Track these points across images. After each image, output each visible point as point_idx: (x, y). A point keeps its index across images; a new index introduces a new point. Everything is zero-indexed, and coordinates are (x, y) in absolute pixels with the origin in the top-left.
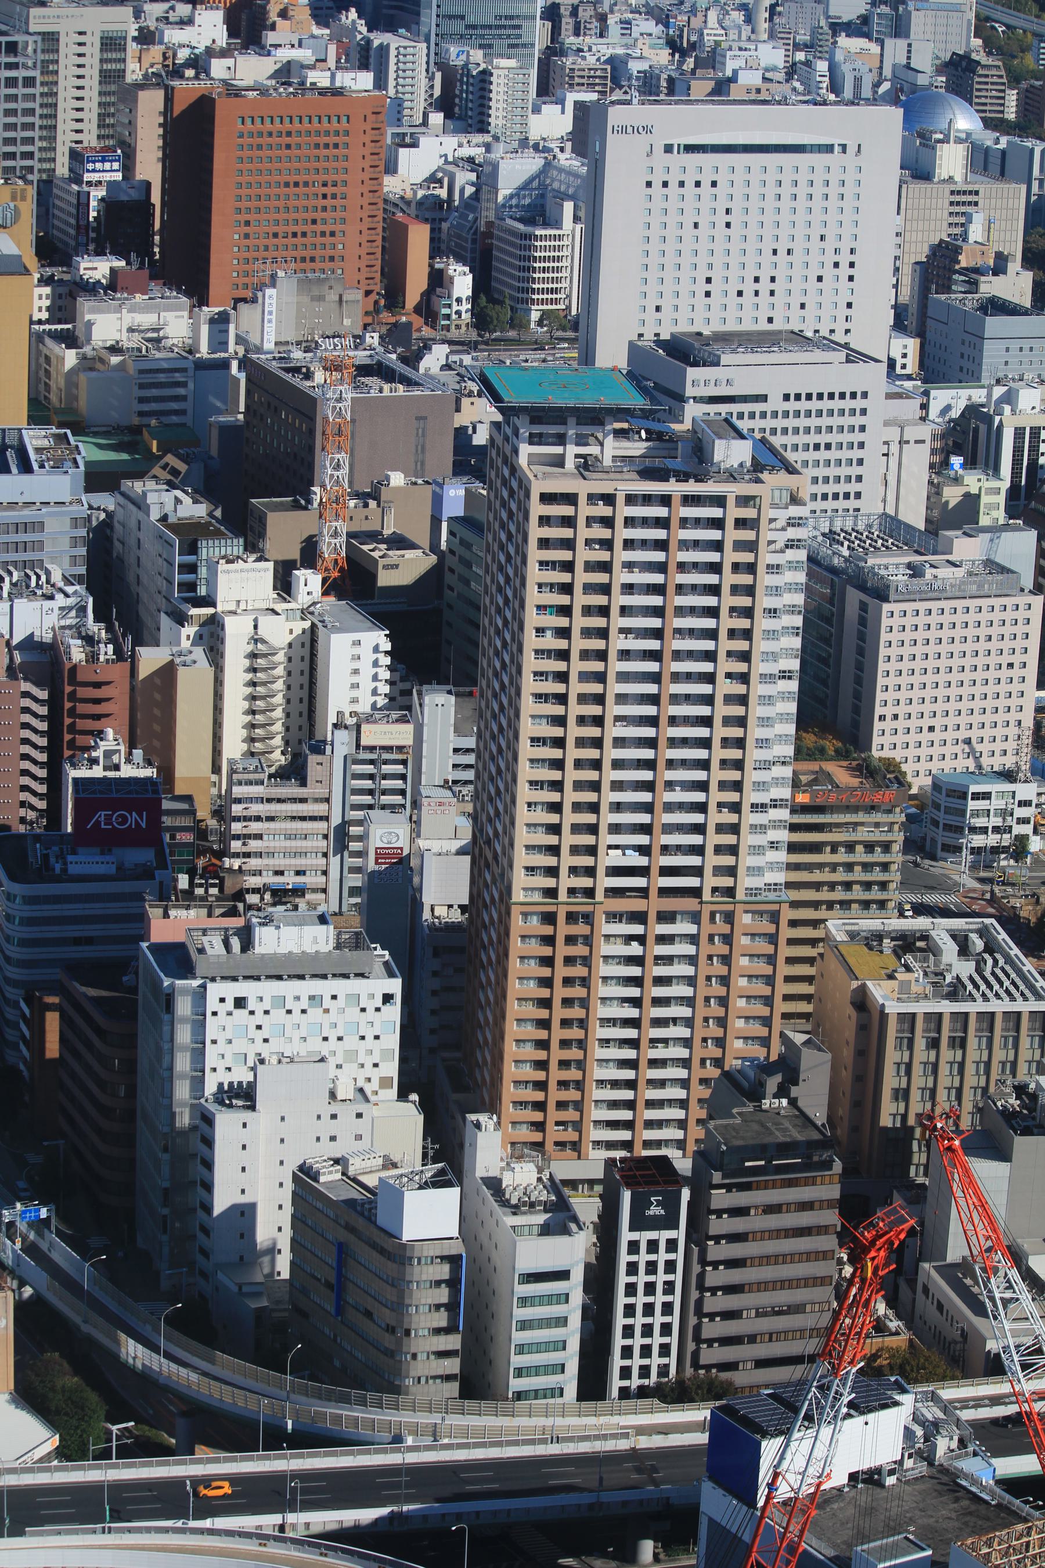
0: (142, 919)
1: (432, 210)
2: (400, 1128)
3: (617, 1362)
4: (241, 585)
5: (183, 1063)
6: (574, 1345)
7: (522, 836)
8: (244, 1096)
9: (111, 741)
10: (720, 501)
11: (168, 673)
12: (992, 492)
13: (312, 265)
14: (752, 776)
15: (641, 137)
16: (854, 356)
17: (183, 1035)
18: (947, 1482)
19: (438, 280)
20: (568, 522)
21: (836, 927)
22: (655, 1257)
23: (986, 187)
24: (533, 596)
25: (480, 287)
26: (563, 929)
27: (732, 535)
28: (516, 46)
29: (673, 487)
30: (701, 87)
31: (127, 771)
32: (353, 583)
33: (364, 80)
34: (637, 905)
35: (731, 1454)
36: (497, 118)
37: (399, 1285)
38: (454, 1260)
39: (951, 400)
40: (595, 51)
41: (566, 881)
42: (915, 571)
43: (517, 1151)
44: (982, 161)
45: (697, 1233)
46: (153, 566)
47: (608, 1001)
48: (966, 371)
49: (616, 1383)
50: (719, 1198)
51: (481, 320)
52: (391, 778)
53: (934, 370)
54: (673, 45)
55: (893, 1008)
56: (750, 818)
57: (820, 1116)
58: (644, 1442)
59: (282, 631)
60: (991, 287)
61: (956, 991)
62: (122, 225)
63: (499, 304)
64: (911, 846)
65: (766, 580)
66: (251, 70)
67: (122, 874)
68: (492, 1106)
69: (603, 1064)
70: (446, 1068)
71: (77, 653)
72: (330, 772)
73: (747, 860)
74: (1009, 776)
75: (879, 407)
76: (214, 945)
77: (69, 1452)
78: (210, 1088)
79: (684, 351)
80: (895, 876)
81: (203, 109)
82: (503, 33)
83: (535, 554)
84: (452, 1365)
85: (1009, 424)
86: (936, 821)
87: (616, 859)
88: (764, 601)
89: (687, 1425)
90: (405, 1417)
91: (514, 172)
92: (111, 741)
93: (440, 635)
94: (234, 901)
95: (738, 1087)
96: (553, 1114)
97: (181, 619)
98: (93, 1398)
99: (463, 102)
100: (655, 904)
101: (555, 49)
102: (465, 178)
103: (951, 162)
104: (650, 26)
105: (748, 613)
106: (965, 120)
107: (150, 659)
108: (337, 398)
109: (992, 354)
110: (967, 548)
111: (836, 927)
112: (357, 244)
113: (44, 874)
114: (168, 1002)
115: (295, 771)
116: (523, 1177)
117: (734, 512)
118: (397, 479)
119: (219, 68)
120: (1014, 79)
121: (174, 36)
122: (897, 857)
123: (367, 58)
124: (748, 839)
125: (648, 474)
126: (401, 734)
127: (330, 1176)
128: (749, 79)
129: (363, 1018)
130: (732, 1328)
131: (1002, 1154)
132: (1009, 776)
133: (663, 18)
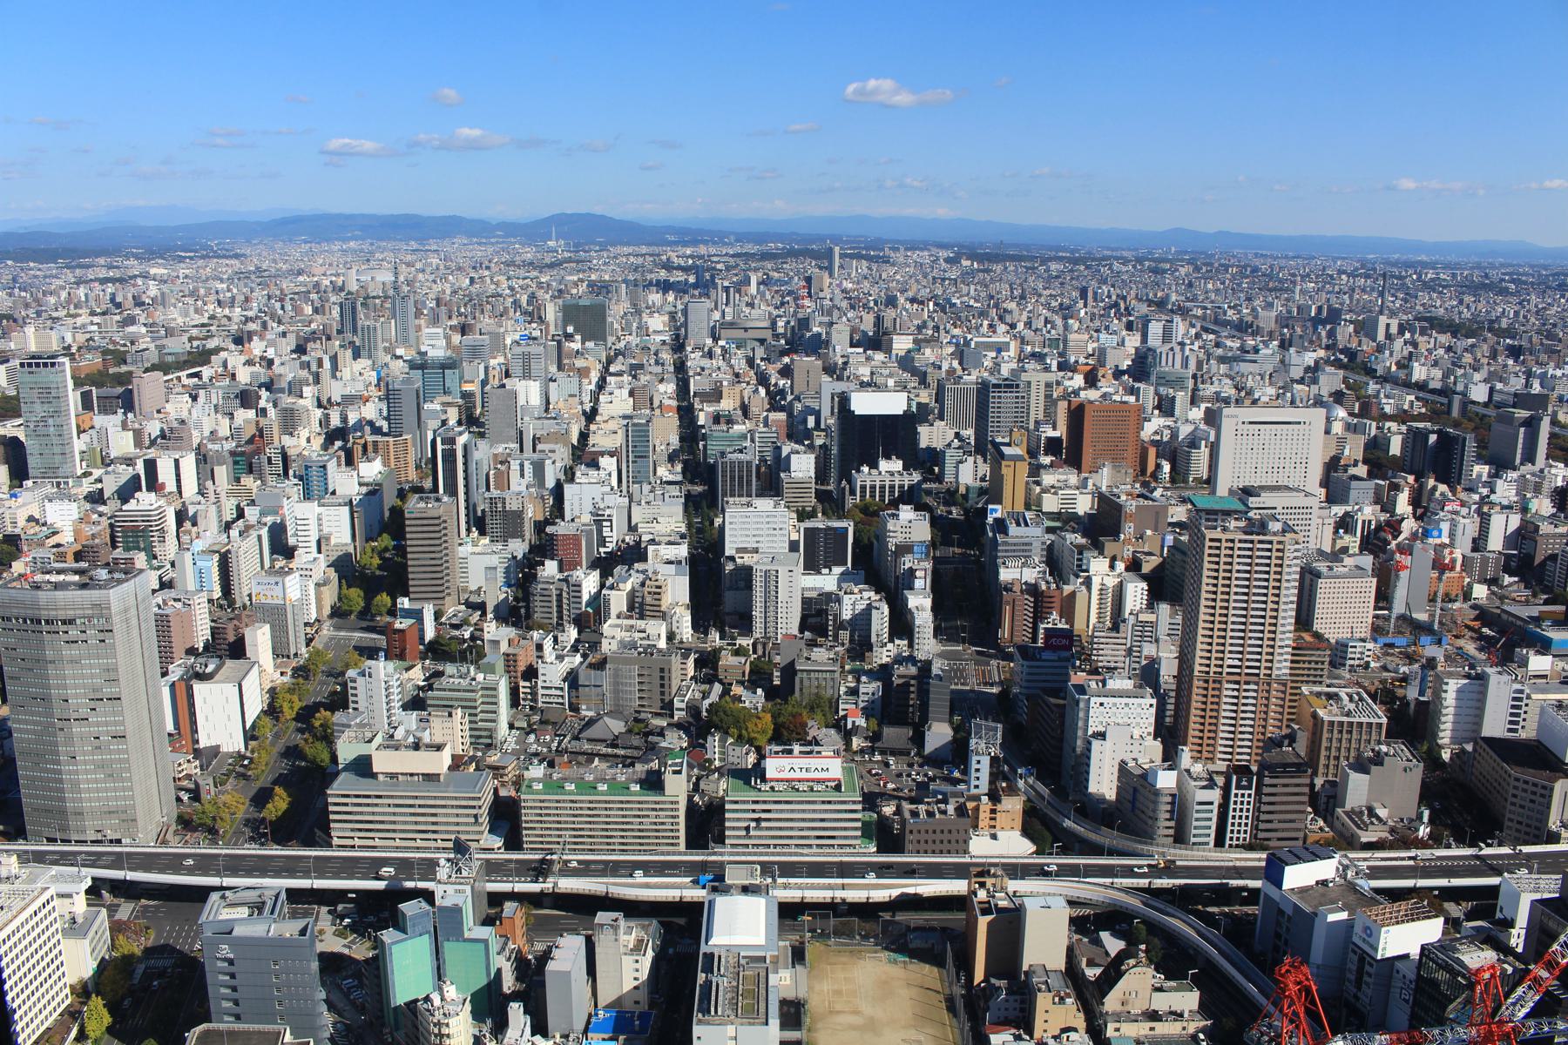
0: (1068, 675)
1: (1155, 443)
2: (1154, 749)
3: (1229, 835)
4: (1098, 566)
5: (1080, 724)
6: (1214, 828)
7: (1199, 653)
8: (1101, 736)
9: (1055, 616)
10: (1271, 542)
11: (1073, 594)
12: (1352, 542)
13: (1116, 460)
14: (1279, 636)
15: (1232, 418)
16: (1307, 494)
17: (1081, 714)
18: (1352, 887)
19: (1158, 466)
20: (1218, 548)
21: (1305, 689)
22: (1242, 800)
23: (1349, 436)
24: (1206, 573)
25: (1172, 469)
26: (1211, 685)
27: (1275, 554)
28: (1183, 388)
29: (1254, 537)
30: (1247, 402)
31: (1060, 626)
32: (1134, 566)
33: (1132, 399)
34: (1237, 678)
35: (1274, 872)
36: (1177, 412)
37: (1155, 803)
38: (1173, 796)
39: (1339, 510)
40: (1208, 390)
41: (1213, 669)
42: (1331, 568)
43: (1195, 760)
44: (1349, 427)
45: (1258, 792)
46: (1070, 561)
47: (1226, 710)
48: (1343, 500)
49: (1228, 842)
50: (1267, 781)
51: (1173, 480)
52: (1147, 631)
53: (1331, 500)
54: (1236, 387)
55: (1326, 718)
56: (1278, 651)
57: (1303, 754)
58: (1238, 864)
59: (1111, 582)
60: (1352, 471)
61: (1348, 714)
62: (1053, 446)
63: (1178, 476)
64: (1331, 663)
65: (1286, 570)
66: (1092, 395)
67: (1060, 660)
68: (1185, 744)
69: (1223, 731)
70: (1170, 734)
71: (1044, 587)
72: (1127, 629)
73: (1276, 665)
74: (1363, 640)
75: (1315, 511)
76: (1093, 685)
77: (1038, 853)
78: (1090, 732)
79: (1248, 492)
80: (1325, 672)
81: (1081, 407)
82: (1178, 383)
83: (1206, 559)
84: (1171, 832)
85: (1360, 518)
86: (1338, 654)
87: (1230, 662)
88: (1286, 577)
89: (1258, 859)
90: (1155, 849)
91: (1185, 431)
92: (1055, 616)
93: (1167, 584)
94: (1095, 671)
95: (1275, 743)
96: (1205, 748)
97: (1077, 576)
98: (1047, 834)
99: (1166, 407)
100: (1244, 678)
101: (1195, 390)
102: (1167, 432)
103: (1337, 428)
104: (1228, 381)
105: (1279, 581)
106: (1341, 413)
107: (1067, 589)
108: (1131, 505)
109: (1353, 494)
110: (1348, 561)
111: (1305, 689)
112: (1131, 454)
113: (1033, 658)
114: (1077, 702)
115: (1115, 627)
116: (1198, 768)
117: (1276, 546)
118: (1149, 532)
119: (1082, 394)
120: (1358, 399)
121: (1067, 383)
122: (1326, 666)
123: (1132, 391)
124: (1277, 658)
125: (1246, 533)
126: (1152, 617)
127: (1131, 764)
128: (1265, 399)
129: (1143, 712)
130: (1269, 826)
131: (1367, 772)
132: (1363, 640)
133: (1232, 379)
